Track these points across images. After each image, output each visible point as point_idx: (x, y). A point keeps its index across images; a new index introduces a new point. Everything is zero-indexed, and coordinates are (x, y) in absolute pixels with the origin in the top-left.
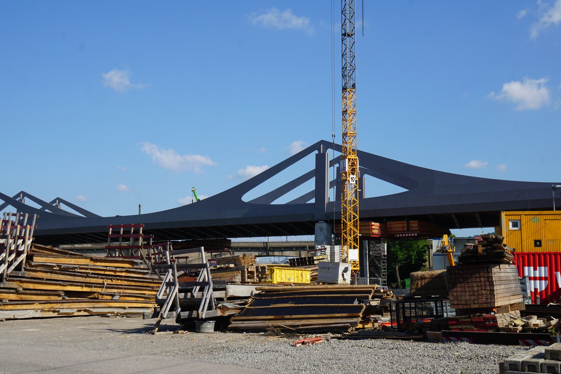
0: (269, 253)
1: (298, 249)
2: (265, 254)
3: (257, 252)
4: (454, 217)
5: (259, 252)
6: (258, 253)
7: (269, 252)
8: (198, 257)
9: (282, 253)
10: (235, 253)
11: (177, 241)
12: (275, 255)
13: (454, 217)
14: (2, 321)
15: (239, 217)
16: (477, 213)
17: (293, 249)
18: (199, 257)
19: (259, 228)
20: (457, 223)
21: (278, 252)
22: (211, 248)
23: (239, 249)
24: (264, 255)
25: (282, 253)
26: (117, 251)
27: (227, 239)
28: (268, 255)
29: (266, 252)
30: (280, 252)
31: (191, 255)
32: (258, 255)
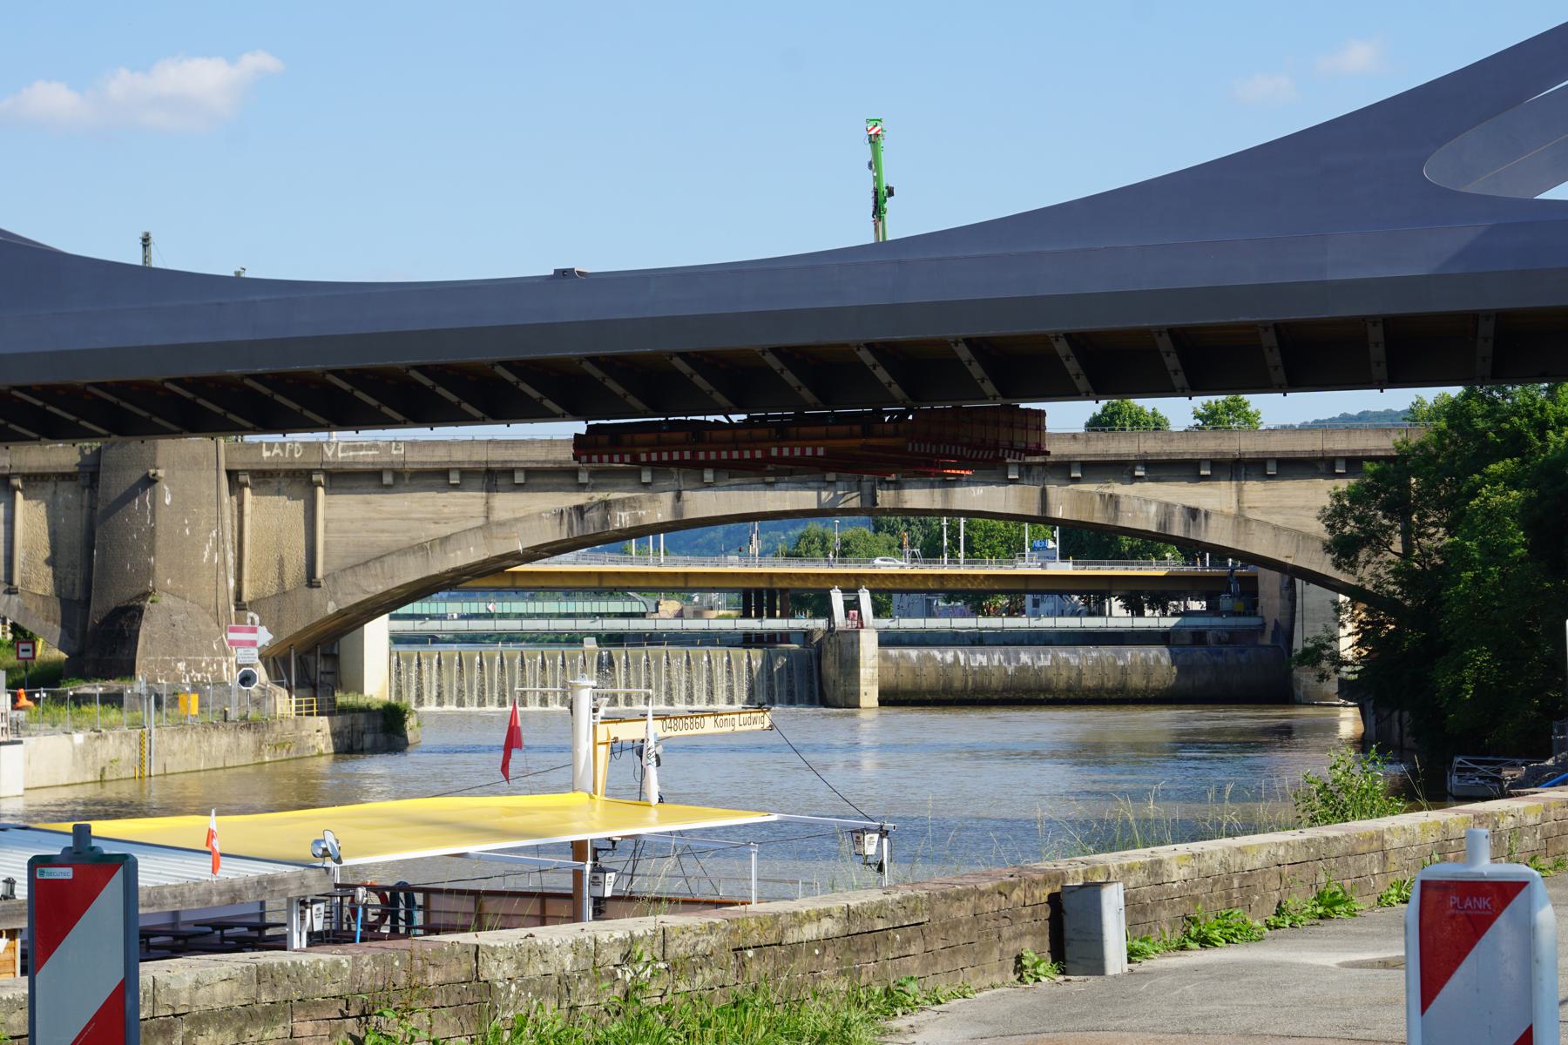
0: (874, 497)
1: (1035, 471)
2: (855, 503)
3: (810, 489)
4: (1062, 348)
5: (819, 489)
6: (815, 493)
7: (879, 492)
8: (481, 522)
9: (946, 497)
10: (686, 494)
11: (702, 418)
12: (908, 506)
13: (1062, 348)
14: (3, 829)
15: (1423, 272)
16: (1160, 334)
17: (1133, 471)
18: (487, 517)
19: (188, 395)
20: (890, 384)
21: (927, 490)
22: (735, 455)
23: (519, 478)
24: (848, 505)
25: (946, 497)
26: (15, 489)
27: (1023, 406)
28: (868, 505)
29: (859, 489)
30: (938, 492)
31: (446, 510)
32: (815, 506)
